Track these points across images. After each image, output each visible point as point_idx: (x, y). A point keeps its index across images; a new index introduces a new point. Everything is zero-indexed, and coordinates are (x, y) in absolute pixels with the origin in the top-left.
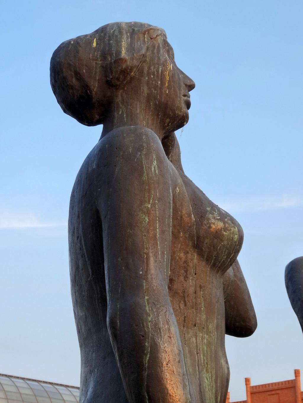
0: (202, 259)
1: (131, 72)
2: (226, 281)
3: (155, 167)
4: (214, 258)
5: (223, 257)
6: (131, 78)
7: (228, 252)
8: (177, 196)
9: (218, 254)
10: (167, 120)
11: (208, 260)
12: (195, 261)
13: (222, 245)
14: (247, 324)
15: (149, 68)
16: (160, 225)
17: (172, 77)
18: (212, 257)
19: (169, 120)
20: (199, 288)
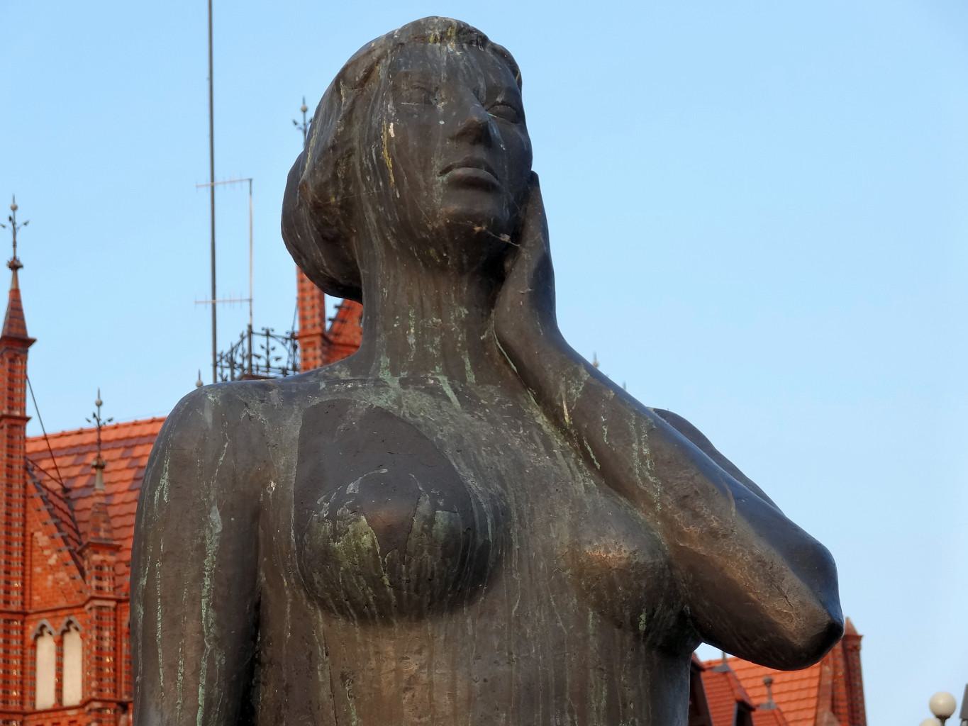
0: (333, 615)
1: (328, 199)
2: (597, 579)
3: (162, 490)
4: (348, 603)
5: (364, 593)
6: (341, 207)
7: (365, 579)
8: (271, 501)
9: (347, 592)
10: (431, 252)
11: (342, 611)
12: (321, 626)
13: (342, 571)
14: (771, 635)
15: (362, 164)
16: (166, 610)
17: (398, 154)
18: (343, 603)
19: (434, 250)
20: (341, 680)
